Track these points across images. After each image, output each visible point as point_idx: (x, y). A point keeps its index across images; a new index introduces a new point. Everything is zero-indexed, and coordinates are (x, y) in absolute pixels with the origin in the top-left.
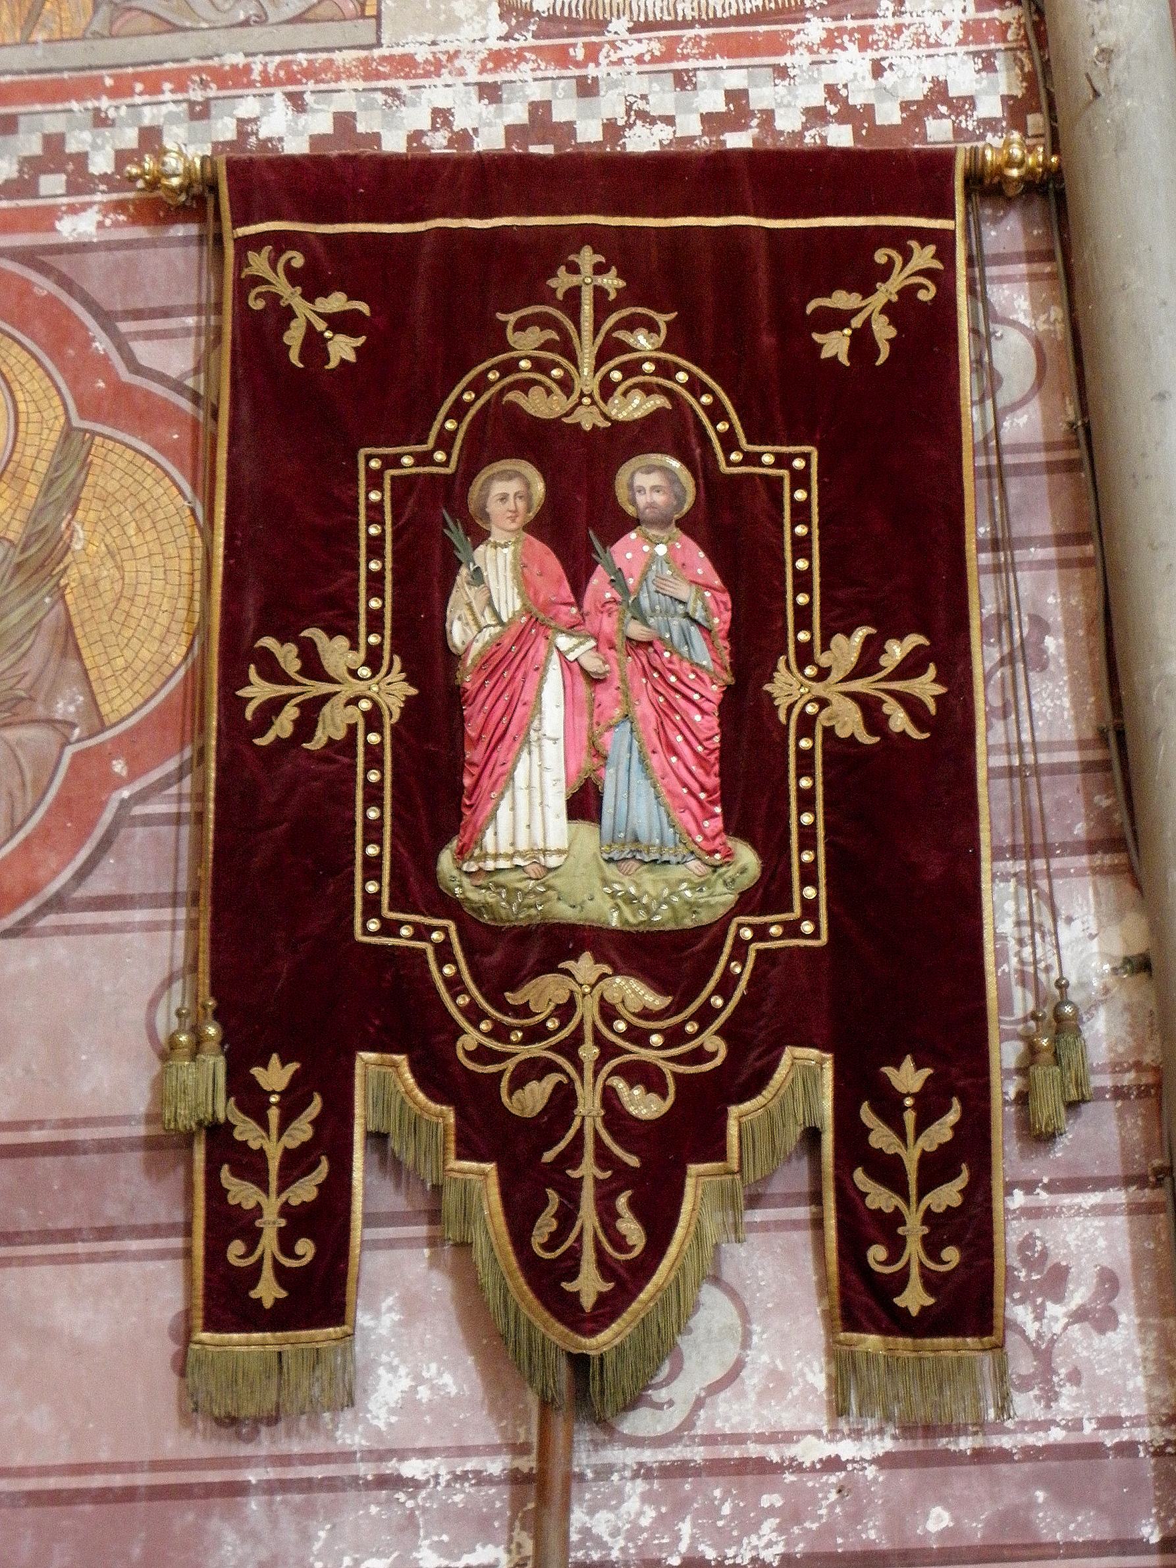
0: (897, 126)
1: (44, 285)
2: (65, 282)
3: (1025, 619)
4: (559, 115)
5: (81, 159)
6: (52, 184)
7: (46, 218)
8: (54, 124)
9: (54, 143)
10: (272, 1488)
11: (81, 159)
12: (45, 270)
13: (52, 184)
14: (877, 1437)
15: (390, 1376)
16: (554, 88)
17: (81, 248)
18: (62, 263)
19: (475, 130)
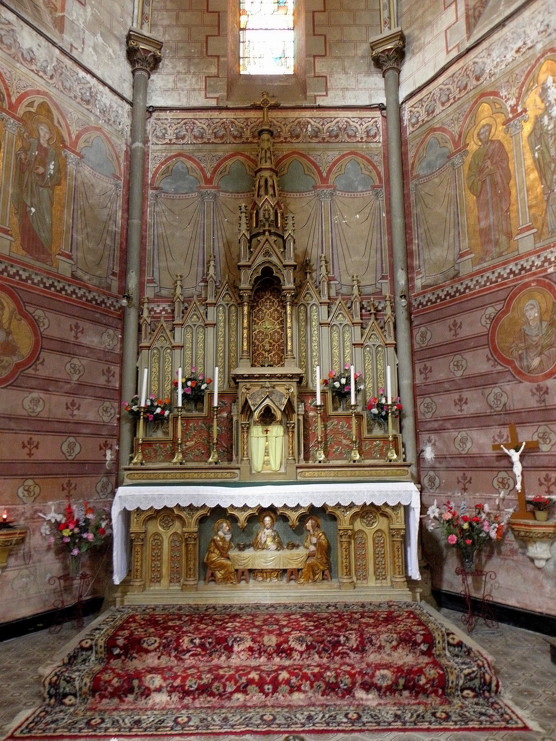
0: (84, 616)
1: (547, 281)
2: (550, 279)
3: (477, 268)
4: (502, 273)
5: (550, 259)
6: (546, 264)
7: (546, 270)
8: (545, 254)
9: (546, 257)
10: (409, 269)
11: (550, 259)
12: (547, 278)
13: (546, 264)
14: (404, 579)
15: (516, 545)
16: (210, 86)
17: (552, 273)
18: (549, 277)
19: (267, 431)
